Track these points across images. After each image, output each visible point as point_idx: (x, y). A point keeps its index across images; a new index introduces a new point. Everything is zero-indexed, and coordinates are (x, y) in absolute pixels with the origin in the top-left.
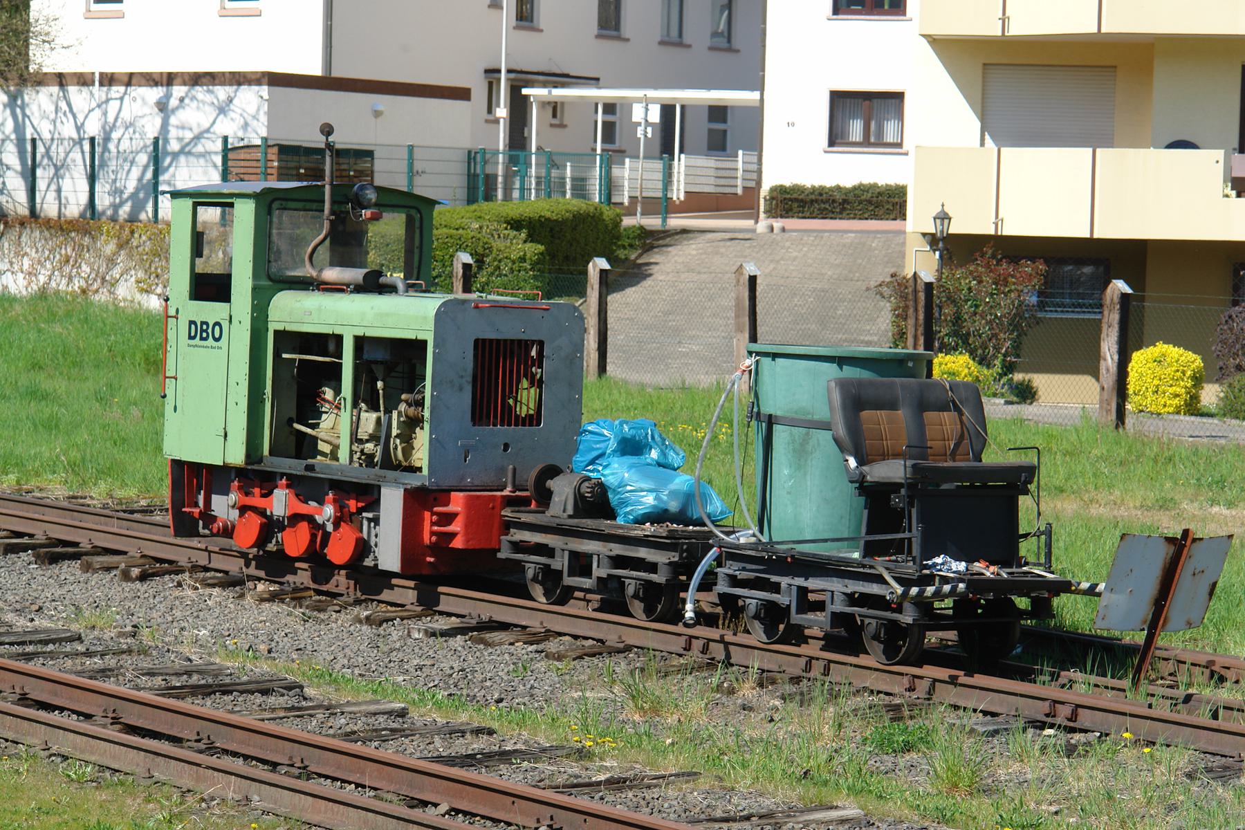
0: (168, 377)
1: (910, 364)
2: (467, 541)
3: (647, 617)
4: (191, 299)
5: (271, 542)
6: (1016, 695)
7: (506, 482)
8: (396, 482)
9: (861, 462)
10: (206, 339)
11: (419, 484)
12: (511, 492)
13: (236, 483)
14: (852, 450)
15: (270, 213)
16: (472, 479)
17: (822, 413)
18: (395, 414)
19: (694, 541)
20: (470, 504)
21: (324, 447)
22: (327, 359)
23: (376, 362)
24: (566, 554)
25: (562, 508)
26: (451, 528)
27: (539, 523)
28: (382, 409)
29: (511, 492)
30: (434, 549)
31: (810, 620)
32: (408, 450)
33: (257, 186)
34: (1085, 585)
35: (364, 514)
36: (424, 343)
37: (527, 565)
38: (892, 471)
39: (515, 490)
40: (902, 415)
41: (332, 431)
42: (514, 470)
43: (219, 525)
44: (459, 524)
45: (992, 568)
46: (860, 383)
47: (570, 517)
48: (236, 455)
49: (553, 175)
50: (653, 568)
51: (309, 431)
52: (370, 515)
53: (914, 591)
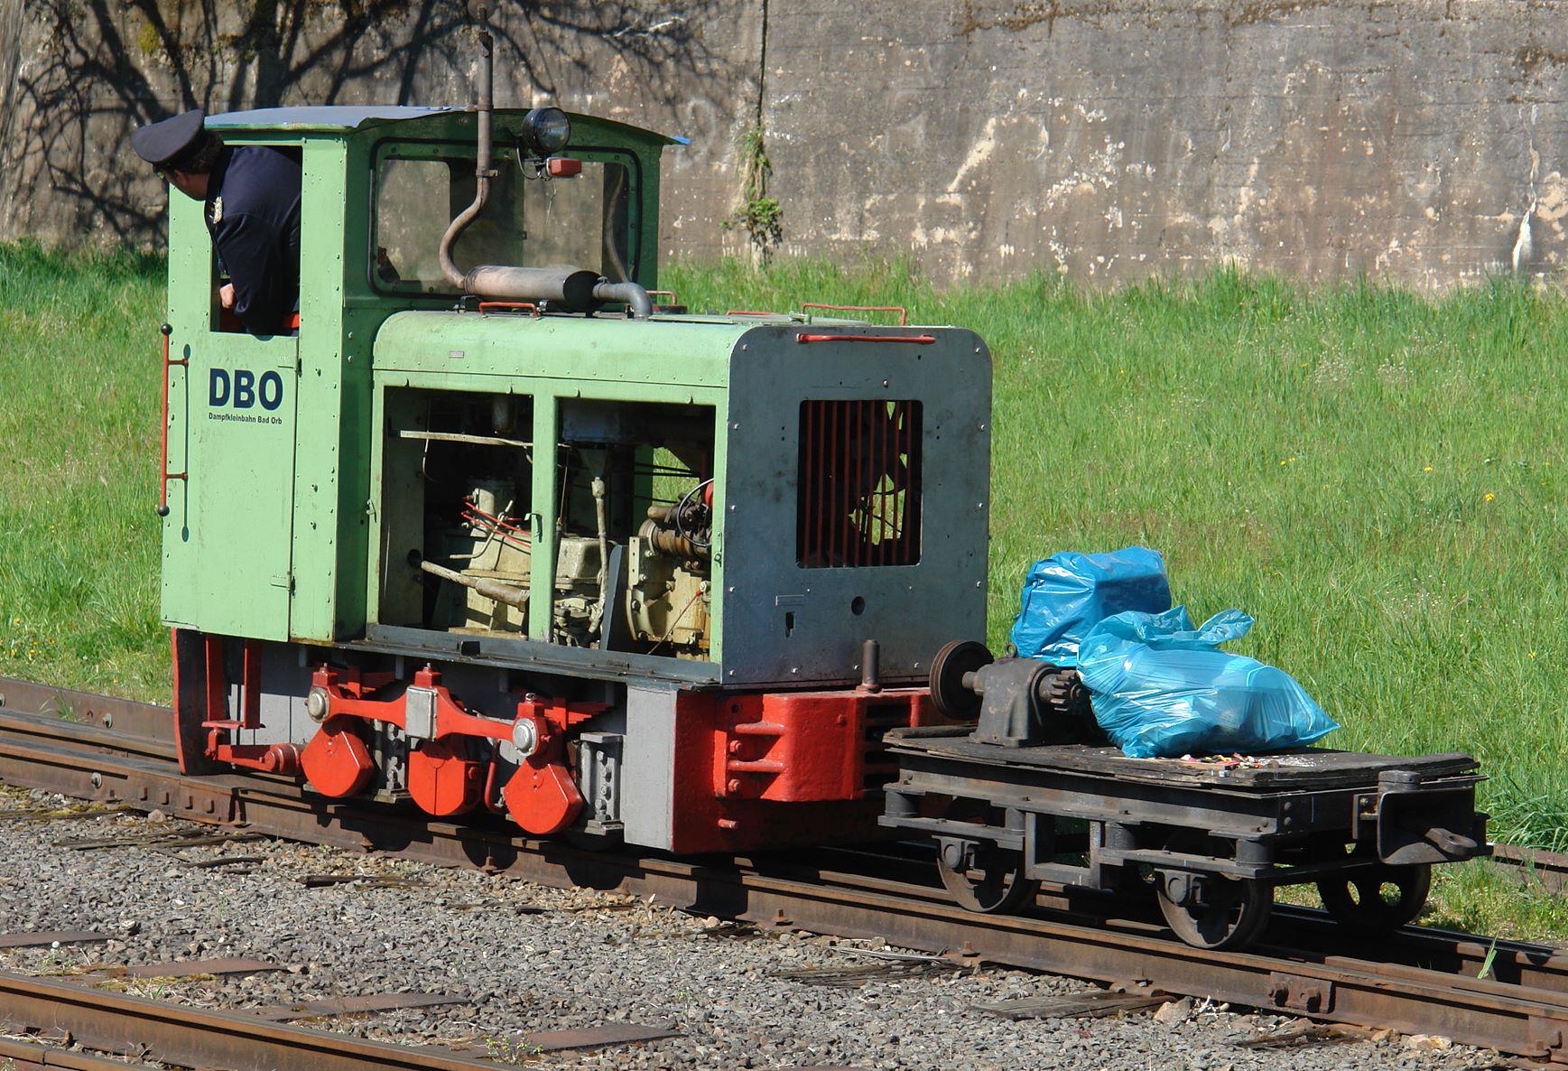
0: (171, 477)
2: (797, 787)
4: (213, 329)
5: (385, 787)
6: (100, 745)
7: (860, 669)
8: (655, 677)
10: (248, 404)
11: (705, 680)
12: (870, 690)
13: (323, 672)
15: (373, 165)
16: (800, 668)
18: (634, 545)
19: (1301, 792)
20: (802, 714)
21: (476, 602)
22: (493, 441)
23: (588, 445)
24: (1031, 821)
25: (1006, 728)
26: (766, 763)
27: (967, 759)
28: (601, 533)
29: (870, 690)
30: (731, 804)
32: (660, 609)
33: (350, 115)
35: (584, 736)
36: (709, 411)
37: (945, 840)
39: (880, 684)
41: (494, 574)
42: (877, 648)
43: (276, 754)
44: (782, 756)
47: (1022, 744)
48: (316, 624)
49: (497, 23)
50: (1225, 847)
51: (453, 575)
52: (597, 738)
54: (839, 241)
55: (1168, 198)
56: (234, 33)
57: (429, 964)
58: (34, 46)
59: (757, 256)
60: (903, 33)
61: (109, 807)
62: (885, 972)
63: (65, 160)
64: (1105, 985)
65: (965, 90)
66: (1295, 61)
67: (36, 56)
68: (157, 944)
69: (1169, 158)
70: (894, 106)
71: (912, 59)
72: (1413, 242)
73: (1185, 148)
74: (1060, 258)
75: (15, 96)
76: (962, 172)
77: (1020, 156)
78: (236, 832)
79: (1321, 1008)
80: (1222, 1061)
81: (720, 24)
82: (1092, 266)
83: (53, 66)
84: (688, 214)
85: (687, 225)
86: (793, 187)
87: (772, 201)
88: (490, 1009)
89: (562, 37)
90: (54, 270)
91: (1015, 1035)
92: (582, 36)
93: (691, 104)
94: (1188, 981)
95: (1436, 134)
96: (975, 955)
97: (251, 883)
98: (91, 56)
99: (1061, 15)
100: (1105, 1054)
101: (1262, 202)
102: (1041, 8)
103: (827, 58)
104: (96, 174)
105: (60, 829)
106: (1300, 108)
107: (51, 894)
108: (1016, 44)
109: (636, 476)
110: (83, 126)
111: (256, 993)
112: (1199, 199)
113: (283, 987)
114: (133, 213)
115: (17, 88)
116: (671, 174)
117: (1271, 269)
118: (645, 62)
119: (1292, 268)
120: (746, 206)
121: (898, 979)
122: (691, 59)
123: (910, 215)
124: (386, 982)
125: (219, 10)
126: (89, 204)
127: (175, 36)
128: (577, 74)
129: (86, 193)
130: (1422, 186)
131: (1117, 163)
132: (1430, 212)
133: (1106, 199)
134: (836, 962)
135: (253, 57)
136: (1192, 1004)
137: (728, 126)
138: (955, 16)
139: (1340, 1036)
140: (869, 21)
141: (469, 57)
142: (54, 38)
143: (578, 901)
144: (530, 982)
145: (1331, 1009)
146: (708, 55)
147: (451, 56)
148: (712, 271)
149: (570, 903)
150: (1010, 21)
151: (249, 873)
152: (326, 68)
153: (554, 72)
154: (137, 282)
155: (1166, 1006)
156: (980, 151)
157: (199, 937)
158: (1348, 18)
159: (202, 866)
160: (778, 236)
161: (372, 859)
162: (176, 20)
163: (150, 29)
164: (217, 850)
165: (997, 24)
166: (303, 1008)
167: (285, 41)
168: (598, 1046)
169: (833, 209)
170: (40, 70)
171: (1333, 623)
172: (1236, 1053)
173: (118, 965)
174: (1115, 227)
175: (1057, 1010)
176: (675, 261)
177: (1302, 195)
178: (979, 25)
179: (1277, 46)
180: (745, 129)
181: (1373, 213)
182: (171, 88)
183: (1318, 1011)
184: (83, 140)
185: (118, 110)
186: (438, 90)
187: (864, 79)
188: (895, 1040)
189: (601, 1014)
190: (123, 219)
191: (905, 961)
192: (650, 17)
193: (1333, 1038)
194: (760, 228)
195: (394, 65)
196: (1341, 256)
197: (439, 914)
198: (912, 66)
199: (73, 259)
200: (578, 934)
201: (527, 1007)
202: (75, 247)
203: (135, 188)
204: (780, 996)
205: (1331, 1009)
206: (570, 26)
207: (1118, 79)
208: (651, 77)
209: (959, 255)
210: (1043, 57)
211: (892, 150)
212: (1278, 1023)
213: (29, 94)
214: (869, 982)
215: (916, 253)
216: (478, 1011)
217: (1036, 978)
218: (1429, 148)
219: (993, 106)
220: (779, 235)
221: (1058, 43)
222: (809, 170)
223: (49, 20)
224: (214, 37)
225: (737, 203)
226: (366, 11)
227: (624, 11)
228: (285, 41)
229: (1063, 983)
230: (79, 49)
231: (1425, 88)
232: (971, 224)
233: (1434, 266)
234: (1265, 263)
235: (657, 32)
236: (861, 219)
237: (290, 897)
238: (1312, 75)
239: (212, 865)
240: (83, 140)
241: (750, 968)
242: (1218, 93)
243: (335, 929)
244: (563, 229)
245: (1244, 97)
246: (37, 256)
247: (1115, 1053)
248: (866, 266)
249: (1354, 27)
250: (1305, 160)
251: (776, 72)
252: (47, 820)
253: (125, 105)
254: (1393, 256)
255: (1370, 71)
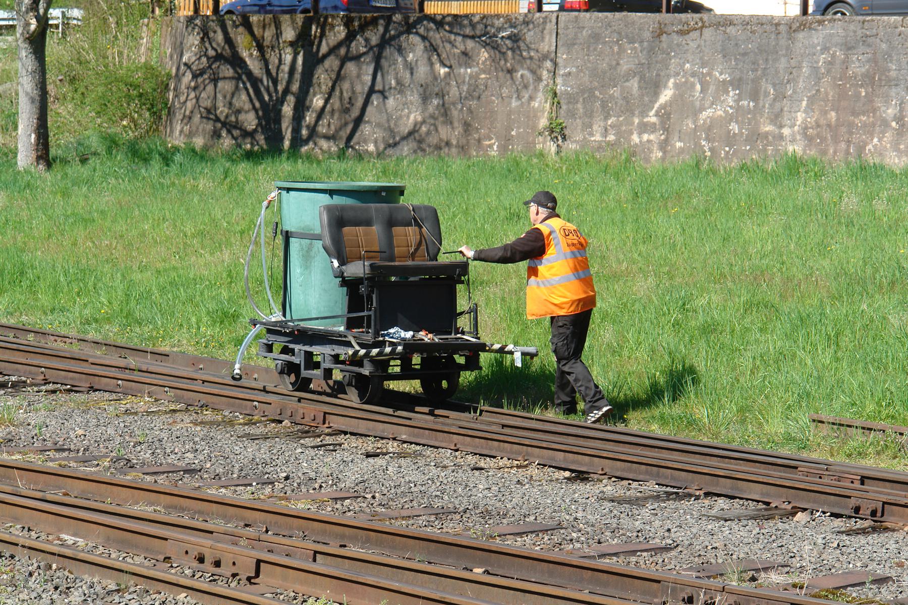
1: (384, 194)
3: (361, 401)
6: (254, 389)
9: (342, 263)
14: (336, 255)
17: (318, 231)
31: (312, 374)
34: (497, 346)
38: (356, 269)
40: (376, 230)
45: (430, 336)
46: (342, 208)
49: (423, 33)
53: (375, 351)
54: (595, 141)
55: (761, 118)
56: (290, 40)
57: (434, 494)
58: (191, 46)
59: (553, 148)
60: (627, 37)
61: (263, 419)
62: (657, 498)
63: (208, 104)
64: (768, 504)
65: (658, 65)
66: (825, 49)
67: (192, 51)
68: (299, 484)
69: (762, 98)
70: (622, 73)
71: (632, 50)
72: (885, 139)
73: (769, 93)
74: (706, 149)
75: (181, 71)
76: (657, 106)
77: (686, 98)
78: (327, 431)
79: (878, 515)
80: (832, 540)
81: (535, 33)
82: (723, 152)
83: (200, 57)
84: (519, 128)
85: (518, 134)
86: (572, 114)
87: (561, 121)
88: (468, 515)
89: (455, 40)
90: (202, 158)
91: (727, 528)
92: (465, 39)
93: (520, 73)
94: (809, 502)
95: (896, 85)
96: (701, 490)
97: (338, 455)
98: (219, 51)
99: (706, 27)
100: (774, 537)
101: (809, 120)
102: (697, 23)
103: (588, 50)
104: (222, 110)
105: (240, 430)
106: (827, 72)
107: (242, 461)
108: (684, 42)
109: (362, 262)
110: (215, 86)
111: (351, 508)
112: (776, 118)
113: (364, 505)
114: (240, 129)
115: (182, 67)
116: (510, 108)
117: (813, 152)
118: (497, 52)
119: (824, 152)
120: (548, 124)
121: (664, 501)
122: (520, 51)
123: (630, 127)
124: (414, 502)
125: (283, 28)
126: (219, 125)
127: (261, 41)
128: (463, 58)
129: (217, 119)
130: (890, 111)
131: (735, 101)
132: (894, 124)
133: (730, 118)
134: (632, 493)
135: (300, 51)
136: (812, 513)
137: (538, 85)
138: (653, 28)
139: (887, 528)
140: (609, 31)
141: (408, 51)
142: (200, 42)
143: (501, 464)
144: (484, 502)
145: (882, 515)
146: (529, 49)
147: (400, 50)
148: (531, 156)
149: (496, 465)
150: (681, 30)
151: (336, 451)
152: (337, 56)
153: (451, 57)
154: (246, 163)
155: (800, 514)
156: (666, 95)
157: (319, 481)
158: (852, 27)
159: (313, 447)
160: (564, 138)
161: (396, 444)
162: (261, 33)
163: (248, 38)
164: (319, 440)
165: (674, 32)
166: (377, 515)
167: (316, 43)
168: (524, 533)
169: (592, 125)
170: (194, 59)
171: (865, 327)
172: (838, 537)
173: (282, 494)
174: (734, 133)
175: (745, 516)
176: (512, 150)
177: (829, 116)
178: (665, 33)
179: (816, 42)
180: (547, 85)
181: (865, 125)
182: (260, 67)
183: (876, 517)
184: (215, 93)
185: (233, 78)
186: (393, 67)
187: (607, 60)
188: (669, 530)
189: (522, 518)
190: (236, 133)
191: (666, 492)
192: (499, 29)
193: (884, 529)
194: (555, 134)
195: (371, 54)
196: (849, 146)
197: (434, 471)
198: (631, 53)
199: (212, 153)
200: (503, 480)
201: (486, 514)
202: (212, 146)
203: (242, 117)
204: (607, 509)
205: (882, 515)
206: (459, 34)
207: (736, 59)
208: (500, 60)
209: (655, 148)
210: (697, 48)
211: (621, 95)
212: (856, 522)
213: (188, 71)
214: (650, 503)
215: (633, 147)
216: (462, 516)
217: (732, 501)
218: (893, 92)
219: (672, 72)
220: (565, 137)
221: (705, 41)
222: (579, 106)
223: (198, 33)
224: (281, 41)
225: (543, 122)
226: (357, 28)
227: (486, 27)
228: (316, 43)
229: (746, 503)
230: (213, 48)
231: (891, 61)
232: (661, 132)
233: (896, 151)
234: (810, 150)
235: (503, 37)
236: (606, 130)
237: (359, 462)
238: (833, 56)
239: (317, 447)
240: (215, 93)
241: (590, 496)
242: (786, 66)
243: (384, 477)
244: (456, 136)
245: (799, 67)
246: (193, 150)
247: (779, 536)
248: (608, 153)
249: (855, 32)
250: (830, 99)
251: (562, 57)
252: (233, 426)
253: (236, 75)
254: (875, 146)
255: (863, 54)
